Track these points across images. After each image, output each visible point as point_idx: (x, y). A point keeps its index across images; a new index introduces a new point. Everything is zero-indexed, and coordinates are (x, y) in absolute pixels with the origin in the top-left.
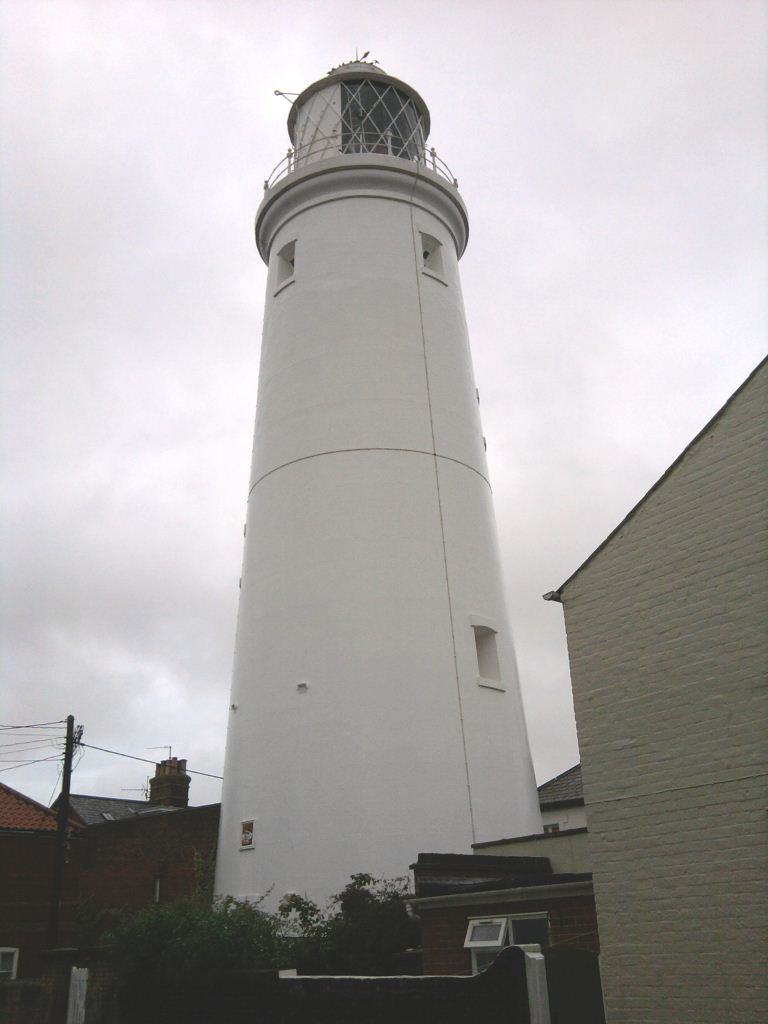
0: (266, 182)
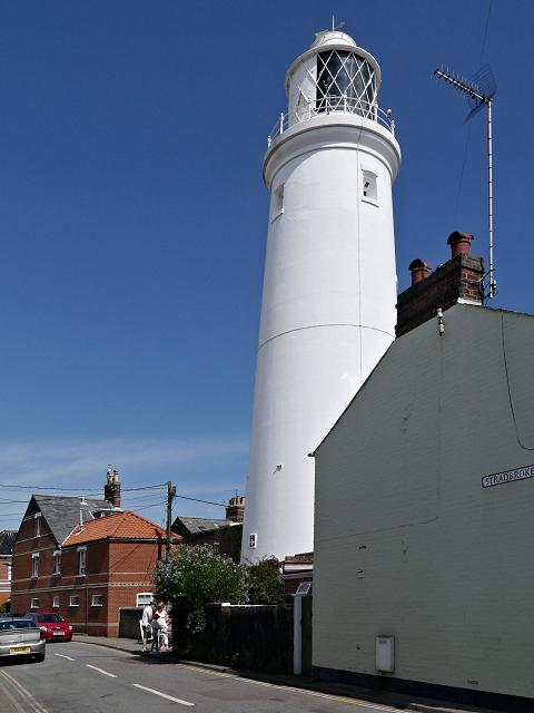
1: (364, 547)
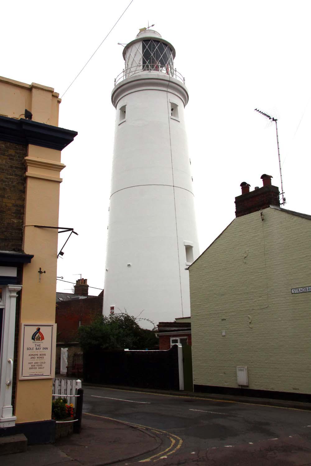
0: (115, 79)
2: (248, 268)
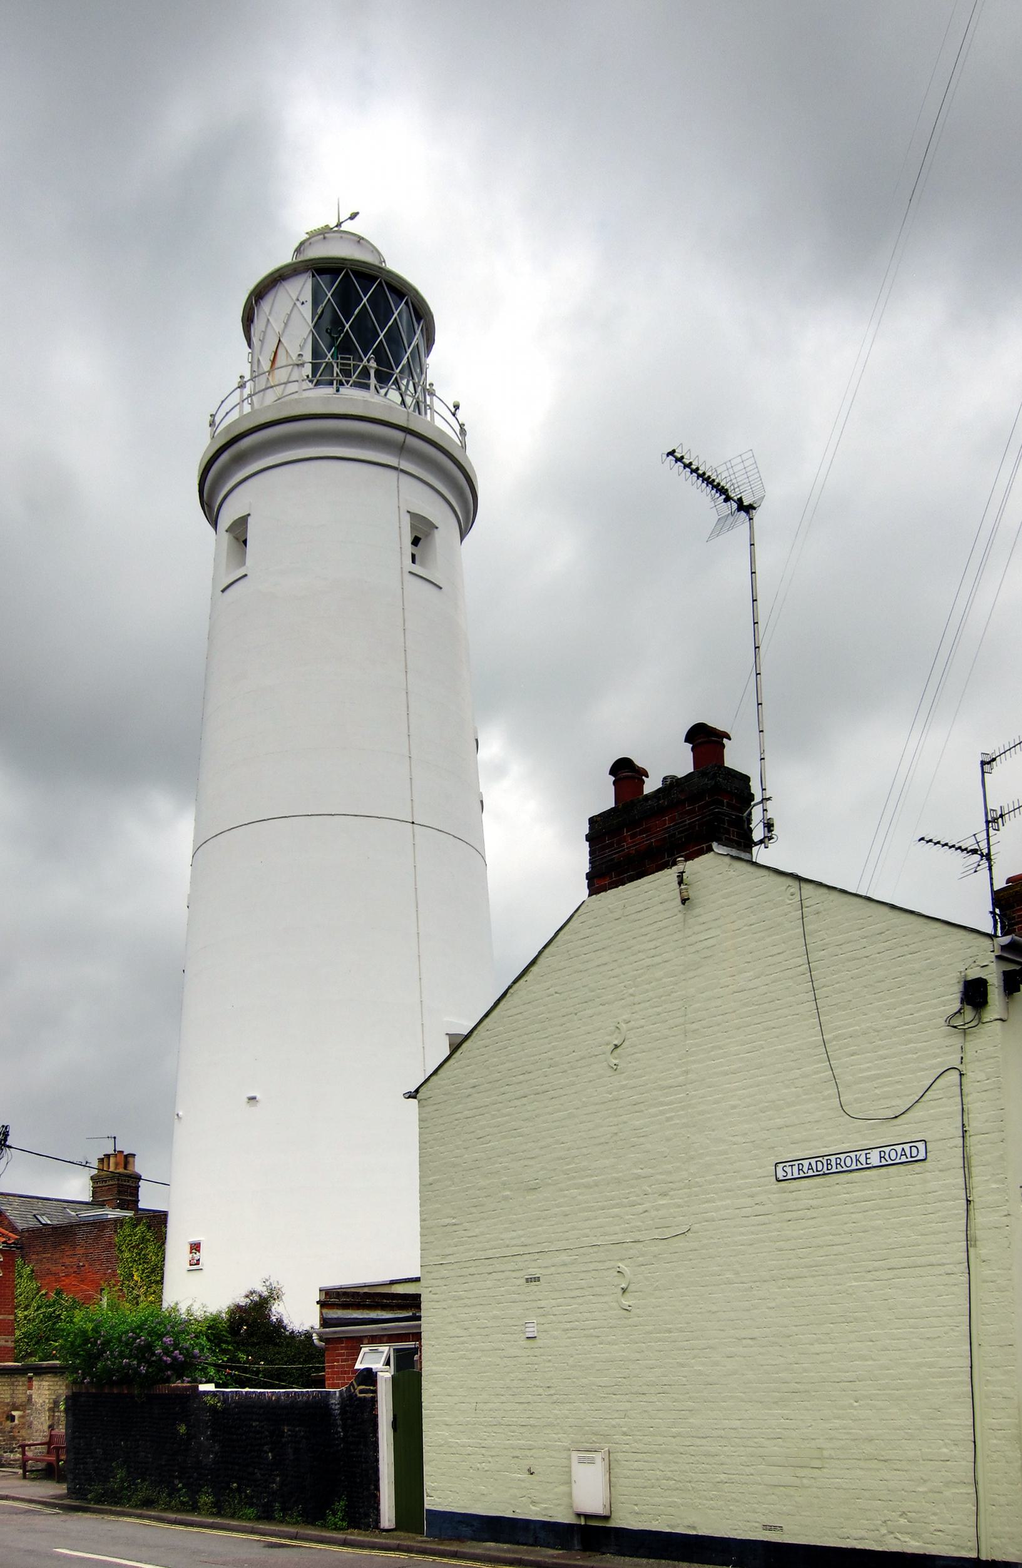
1: (538, 1279)
2: (623, 1087)
